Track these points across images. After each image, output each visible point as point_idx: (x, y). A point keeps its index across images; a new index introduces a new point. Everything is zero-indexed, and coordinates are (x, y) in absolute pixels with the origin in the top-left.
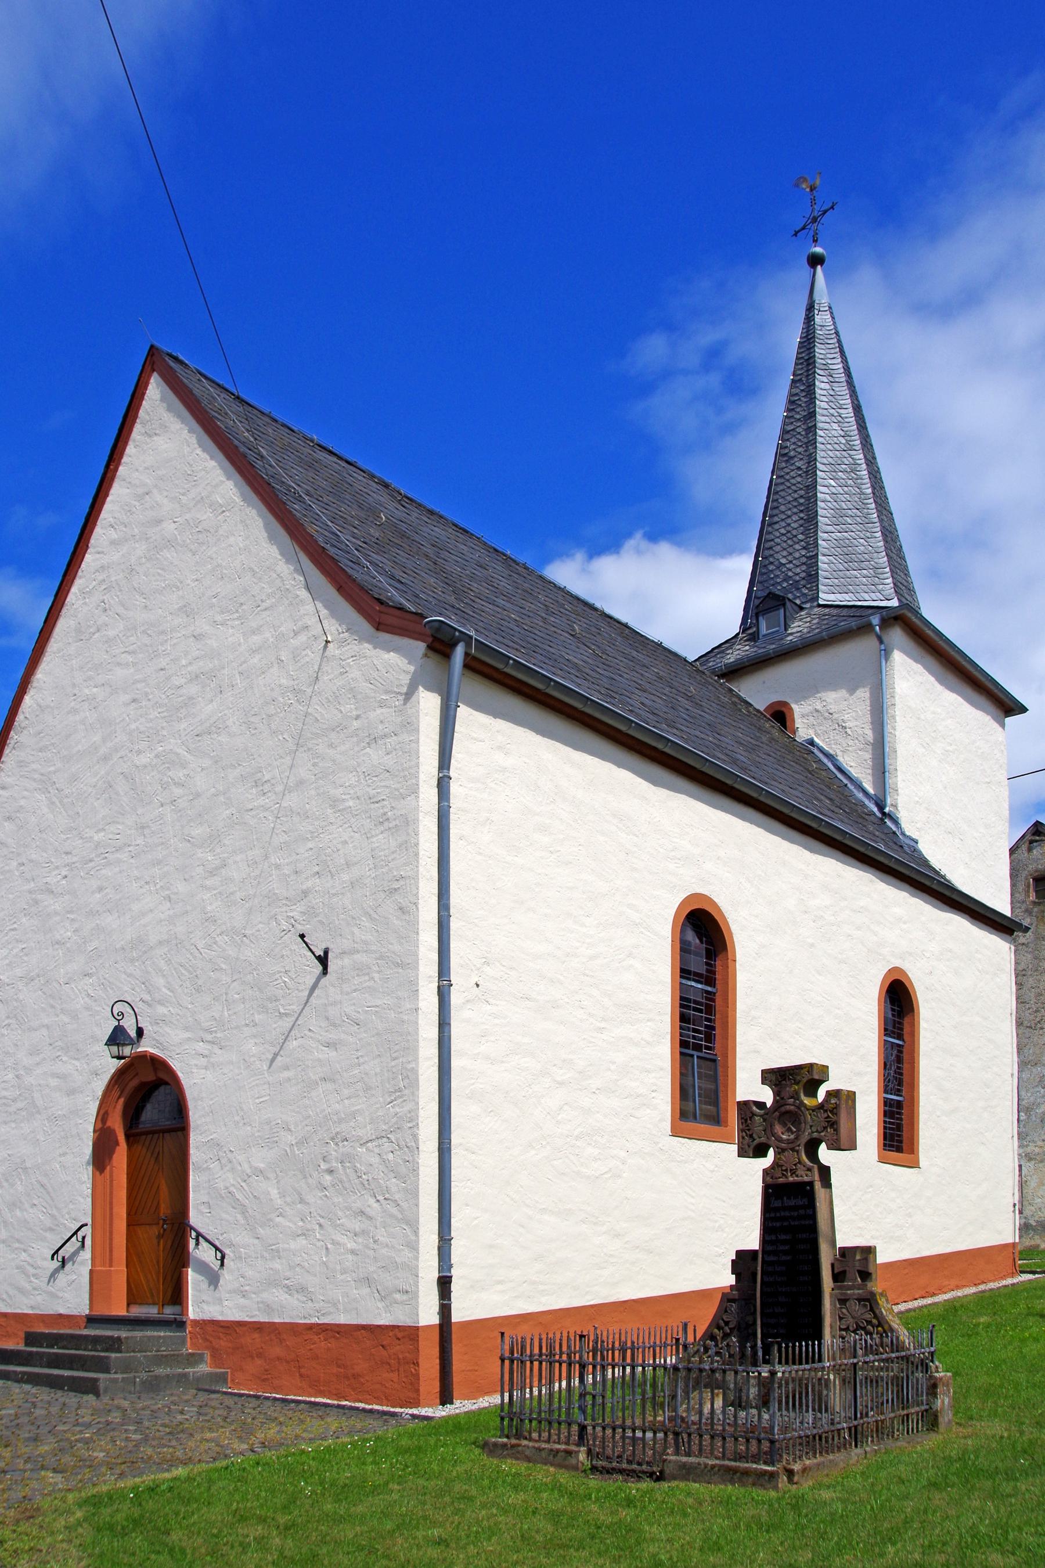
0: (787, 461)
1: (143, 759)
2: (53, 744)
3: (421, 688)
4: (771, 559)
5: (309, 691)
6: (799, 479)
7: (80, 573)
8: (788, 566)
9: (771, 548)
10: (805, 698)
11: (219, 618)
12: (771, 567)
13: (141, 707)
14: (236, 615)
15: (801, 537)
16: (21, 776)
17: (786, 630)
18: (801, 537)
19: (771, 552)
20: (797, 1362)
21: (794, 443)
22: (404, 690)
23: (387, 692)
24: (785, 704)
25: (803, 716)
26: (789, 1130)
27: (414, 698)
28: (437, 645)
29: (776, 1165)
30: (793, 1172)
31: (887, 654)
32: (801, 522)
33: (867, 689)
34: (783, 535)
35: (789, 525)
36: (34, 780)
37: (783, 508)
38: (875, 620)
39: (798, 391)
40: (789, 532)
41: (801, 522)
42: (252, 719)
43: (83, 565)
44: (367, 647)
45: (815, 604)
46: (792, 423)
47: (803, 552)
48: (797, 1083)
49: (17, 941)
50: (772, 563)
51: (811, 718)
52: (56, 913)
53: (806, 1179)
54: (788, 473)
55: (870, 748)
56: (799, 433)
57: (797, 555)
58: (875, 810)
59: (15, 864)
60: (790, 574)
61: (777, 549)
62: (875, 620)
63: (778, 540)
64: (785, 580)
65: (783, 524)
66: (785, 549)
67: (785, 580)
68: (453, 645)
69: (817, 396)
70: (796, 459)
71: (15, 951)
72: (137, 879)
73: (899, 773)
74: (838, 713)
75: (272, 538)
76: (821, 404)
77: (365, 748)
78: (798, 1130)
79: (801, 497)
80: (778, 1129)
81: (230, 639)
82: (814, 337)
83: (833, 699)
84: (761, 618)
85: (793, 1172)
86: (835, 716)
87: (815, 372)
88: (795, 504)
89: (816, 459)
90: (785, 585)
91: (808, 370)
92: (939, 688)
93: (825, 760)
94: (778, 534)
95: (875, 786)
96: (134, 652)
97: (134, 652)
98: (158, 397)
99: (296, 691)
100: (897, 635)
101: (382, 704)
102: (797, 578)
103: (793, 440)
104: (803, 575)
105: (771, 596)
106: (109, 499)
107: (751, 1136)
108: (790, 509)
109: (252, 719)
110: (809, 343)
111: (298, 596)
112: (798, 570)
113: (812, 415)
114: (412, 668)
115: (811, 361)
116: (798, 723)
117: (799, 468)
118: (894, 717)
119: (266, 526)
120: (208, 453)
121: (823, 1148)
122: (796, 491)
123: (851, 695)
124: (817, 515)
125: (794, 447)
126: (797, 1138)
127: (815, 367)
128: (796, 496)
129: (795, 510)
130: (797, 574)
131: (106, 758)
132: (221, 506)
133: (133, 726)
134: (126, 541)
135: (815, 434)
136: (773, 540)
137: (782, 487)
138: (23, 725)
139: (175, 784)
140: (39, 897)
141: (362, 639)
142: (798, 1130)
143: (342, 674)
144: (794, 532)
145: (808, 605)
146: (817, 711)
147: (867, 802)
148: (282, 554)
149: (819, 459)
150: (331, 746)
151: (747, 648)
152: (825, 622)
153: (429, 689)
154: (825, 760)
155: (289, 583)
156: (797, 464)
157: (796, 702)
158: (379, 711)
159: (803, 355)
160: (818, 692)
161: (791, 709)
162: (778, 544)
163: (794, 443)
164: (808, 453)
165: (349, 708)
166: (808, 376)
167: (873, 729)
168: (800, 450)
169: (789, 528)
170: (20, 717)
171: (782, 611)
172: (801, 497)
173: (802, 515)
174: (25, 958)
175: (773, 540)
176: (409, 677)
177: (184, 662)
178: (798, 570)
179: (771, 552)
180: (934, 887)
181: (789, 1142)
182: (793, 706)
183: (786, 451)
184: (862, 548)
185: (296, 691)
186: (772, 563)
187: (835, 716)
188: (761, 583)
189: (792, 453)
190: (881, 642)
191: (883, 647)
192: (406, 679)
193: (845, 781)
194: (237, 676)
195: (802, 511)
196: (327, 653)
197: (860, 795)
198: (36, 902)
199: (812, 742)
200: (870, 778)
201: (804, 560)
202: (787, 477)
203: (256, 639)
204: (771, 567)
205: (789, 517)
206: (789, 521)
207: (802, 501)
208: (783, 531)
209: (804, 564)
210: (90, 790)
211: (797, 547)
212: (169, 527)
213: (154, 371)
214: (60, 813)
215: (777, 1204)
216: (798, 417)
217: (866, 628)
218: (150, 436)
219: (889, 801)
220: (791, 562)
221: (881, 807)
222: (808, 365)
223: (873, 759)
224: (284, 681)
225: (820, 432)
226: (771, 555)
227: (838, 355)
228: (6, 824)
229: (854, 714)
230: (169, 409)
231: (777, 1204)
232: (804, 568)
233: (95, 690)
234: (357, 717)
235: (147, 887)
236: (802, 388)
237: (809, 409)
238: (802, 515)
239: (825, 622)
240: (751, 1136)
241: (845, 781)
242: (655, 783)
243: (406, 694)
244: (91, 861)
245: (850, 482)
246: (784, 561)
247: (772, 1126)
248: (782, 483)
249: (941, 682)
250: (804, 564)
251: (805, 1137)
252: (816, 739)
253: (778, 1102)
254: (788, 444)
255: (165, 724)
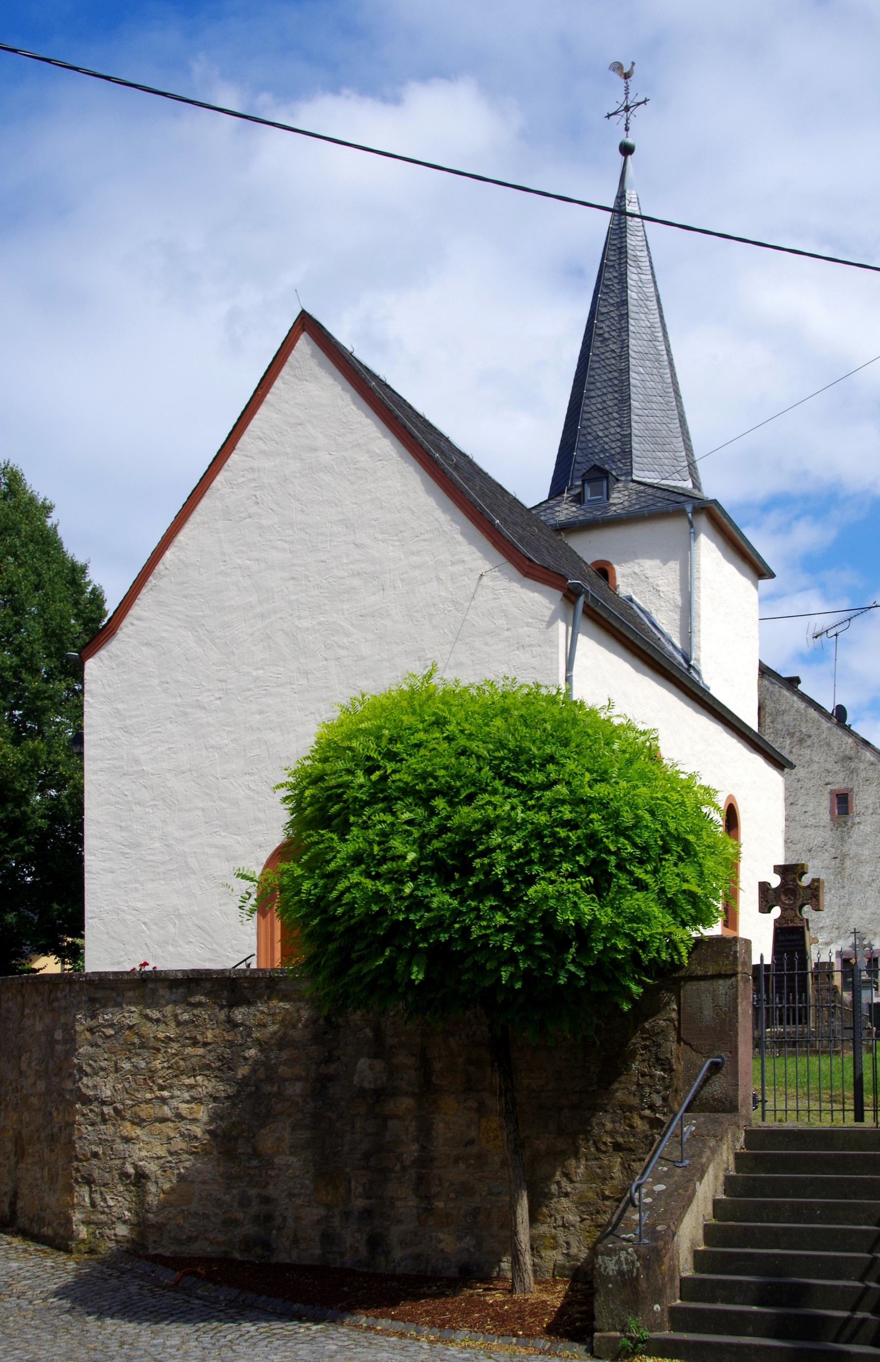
0: (602, 342)
1: (304, 624)
2: (201, 595)
3: (559, 621)
4: (589, 430)
5: (467, 604)
6: (613, 361)
7: (225, 466)
8: (604, 439)
9: (588, 420)
10: (626, 561)
11: (380, 536)
12: (589, 437)
13: (301, 585)
14: (396, 538)
15: (615, 415)
16: (161, 613)
17: (608, 499)
18: (615, 415)
19: (589, 423)
20: (785, 1021)
21: (608, 326)
22: (547, 619)
23: (532, 618)
24: (608, 564)
25: (623, 576)
26: (789, 899)
27: (554, 626)
28: (568, 594)
29: (781, 917)
30: (792, 921)
31: (696, 535)
32: (615, 401)
33: (678, 562)
34: (600, 410)
35: (605, 402)
36: (179, 619)
37: (599, 385)
38: (689, 508)
39: (611, 276)
40: (605, 408)
41: (615, 401)
42: (415, 614)
43: (229, 461)
44: (515, 586)
45: (629, 478)
46: (606, 306)
47: (618, 430)
48: (795, 873)
49: (162, 741)
50: (589, 433)
51: (630, 579)
52: (209, 724)
53: (800, 925)
54: (603, 353)
55: (678, 610)
56: (613, 317)
57: (612, 431)
58: (682, 661)
59: (157, 681)
60: (606, 447)
61: (595, 421)
62: (689, 508)
63: (595, 414)
64: (601, 451)
65: (599, 400)
66: (601, 423)
67: (601, 451)
68: (578, 596)
69: (629, 286)
70: (610, 342)
71: (160, 749)
72: (301, 709)
73: (701, 634)
74: (654, 578)
75: (428, 491)
76: (632, 295)
77: (514, 650)
78: (795, 899)
79: (616, 378)
80: (783, 898)
81: (391, 554)
82: (625, 227)
83: (650, 566)
84: (586, 485)
85: (792, 921)
86: (651, 580)
87: (626, 262)
88: (610, 384)
89: (628, 346)
90: (602, 456)
91: (620, 259)
92: (724, 562)
93: (642, 615)
94: (595, 408)
95: (682, 640)
96: (291, 542)
97: (291, 542)
98: (309, 352)
99: (455, 603)
100: (703, 522)
101: (528, 625)
102: (613, 452)
103: (607, 323)
104: (618, 450)
105: (596, 468)
106: (256, 416)
107: (767, 901)
108: (605, 387)
109: (415, 614)
110: (621, 232)
111: (454, 538)
112: (613, 445)
113: (625, 303)
114: (553, 607)
115: (623, 250)
116: (619, 581)
117: (613, 351)
118: (699, 588)
119: (423, 481)
120: (363, 411)
121: (806, 908)
122: (610, 372)
123: (664, 565)
124: (630, 398)
125: (608, 329)
126: (794, 903)
127: (626, 257)
128: (610, 376)
129: (610, 389)
130: (613, 448)
131: (263, 616)
132: (378, 455)
133: (293, 597)
134: (278, 455)
135: (628, 322)
136: (590, 413)
137: (597, 365)
138: (163, 573)
139: (339, 646)
140: (188, 710)
141: (511, 580)
142: (795, 899)
143: (494, 599)
144: (610, 410)
145: (623, 478)
146: (635, 573)
147: (675, 654)
148: (438, 505)
149: (631, 347)
150: (486, 644)
151: (574, 509)
152: (643, 499)
153: (562, 621)
154: (642, 615)
155: (447, 527)
156: (611, 346)
157: (618, 564)
158: (526, 629)
159: (616, 242)
160: (637, 558)
161: (613, 569)
162: (595, 418)
163: (608, 326)
164: (620, 339)
165: (501, 622)
166: (620, 264)
167: (682, 596)
168: (614, 333)
169: (605, 405)
170: (160, 567)
171: (605, 483)
172: (616, 378)
173: (616, 395)
174: (174, 756)
175: (590, 413)
176: (551, 612)
177: (345, 561)
178: (613, 445)
179: (589, 423)
180: (751, 736)
181: (789, 905)
182: (615, 566)
183: (601, 332)
184: (664, 432)
185: (455, 603)
186: (589, 433)
187: (651, 580)
188: (580, 449)
189: (606, 335)
190: (692, 526)
191: (692, 530)
192: (548, 613)
193: (659, 635)
194: (399, 581)
195: (616, 392)
196: (482, 582)
197: (670, 648)
198: (185, 714)
199: (631, 600)
200: (678, 635)
201: (619, 437)
202: (603, 357)
203: (415, 559)
204: (589, 437)
205: (605, 394)
206: (605, 398)
207: (616, 382)
208: (599, 406)
209: (618, 440)
210: (246, 637)
211: (612, 423)
212: (324, 458)
213: (304, 330)
214: (212, 649)
215: (782, 938)
216: (611, 301)
217: (680, 513)
218: (300, 380)
219: (694, 656)
220: (607, 436)
221: (687, 661)
222: (620, 253)
223: (681, 620)
224: (442, 593)
225: (631, 321)
226: (589, 427)
227: (645, 248)
228: (143, 648)
229: (666, 581)
230: (320, 365)
231: (782, 938)
232: (619, 444)
233: (248, 562)
234: (508, 630)
235: (313, 716)
236: (615, 275)
237: (622, 297)
238: (616, 395)
239: (643, 499)
240: (767, 901)
241: (659, 635)
242: (638, 670)
243: (548, 622)
244: (249, 690)
245: (655, 371)
246: (600, 434)
247: (779, 896)
248: (598, 362)
249: (725, 556)
250: (618, 440)
251: (799, 903)
252: (634, 597)
253: (782, 885)
254: (603, 325)
255: (327, 602)
